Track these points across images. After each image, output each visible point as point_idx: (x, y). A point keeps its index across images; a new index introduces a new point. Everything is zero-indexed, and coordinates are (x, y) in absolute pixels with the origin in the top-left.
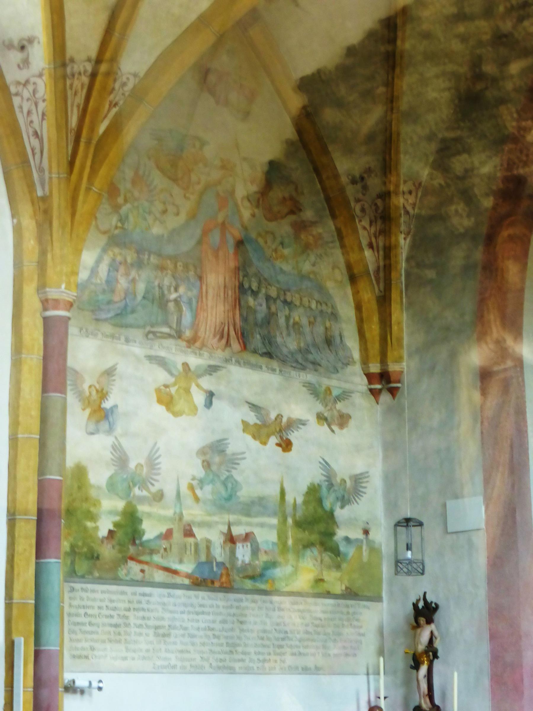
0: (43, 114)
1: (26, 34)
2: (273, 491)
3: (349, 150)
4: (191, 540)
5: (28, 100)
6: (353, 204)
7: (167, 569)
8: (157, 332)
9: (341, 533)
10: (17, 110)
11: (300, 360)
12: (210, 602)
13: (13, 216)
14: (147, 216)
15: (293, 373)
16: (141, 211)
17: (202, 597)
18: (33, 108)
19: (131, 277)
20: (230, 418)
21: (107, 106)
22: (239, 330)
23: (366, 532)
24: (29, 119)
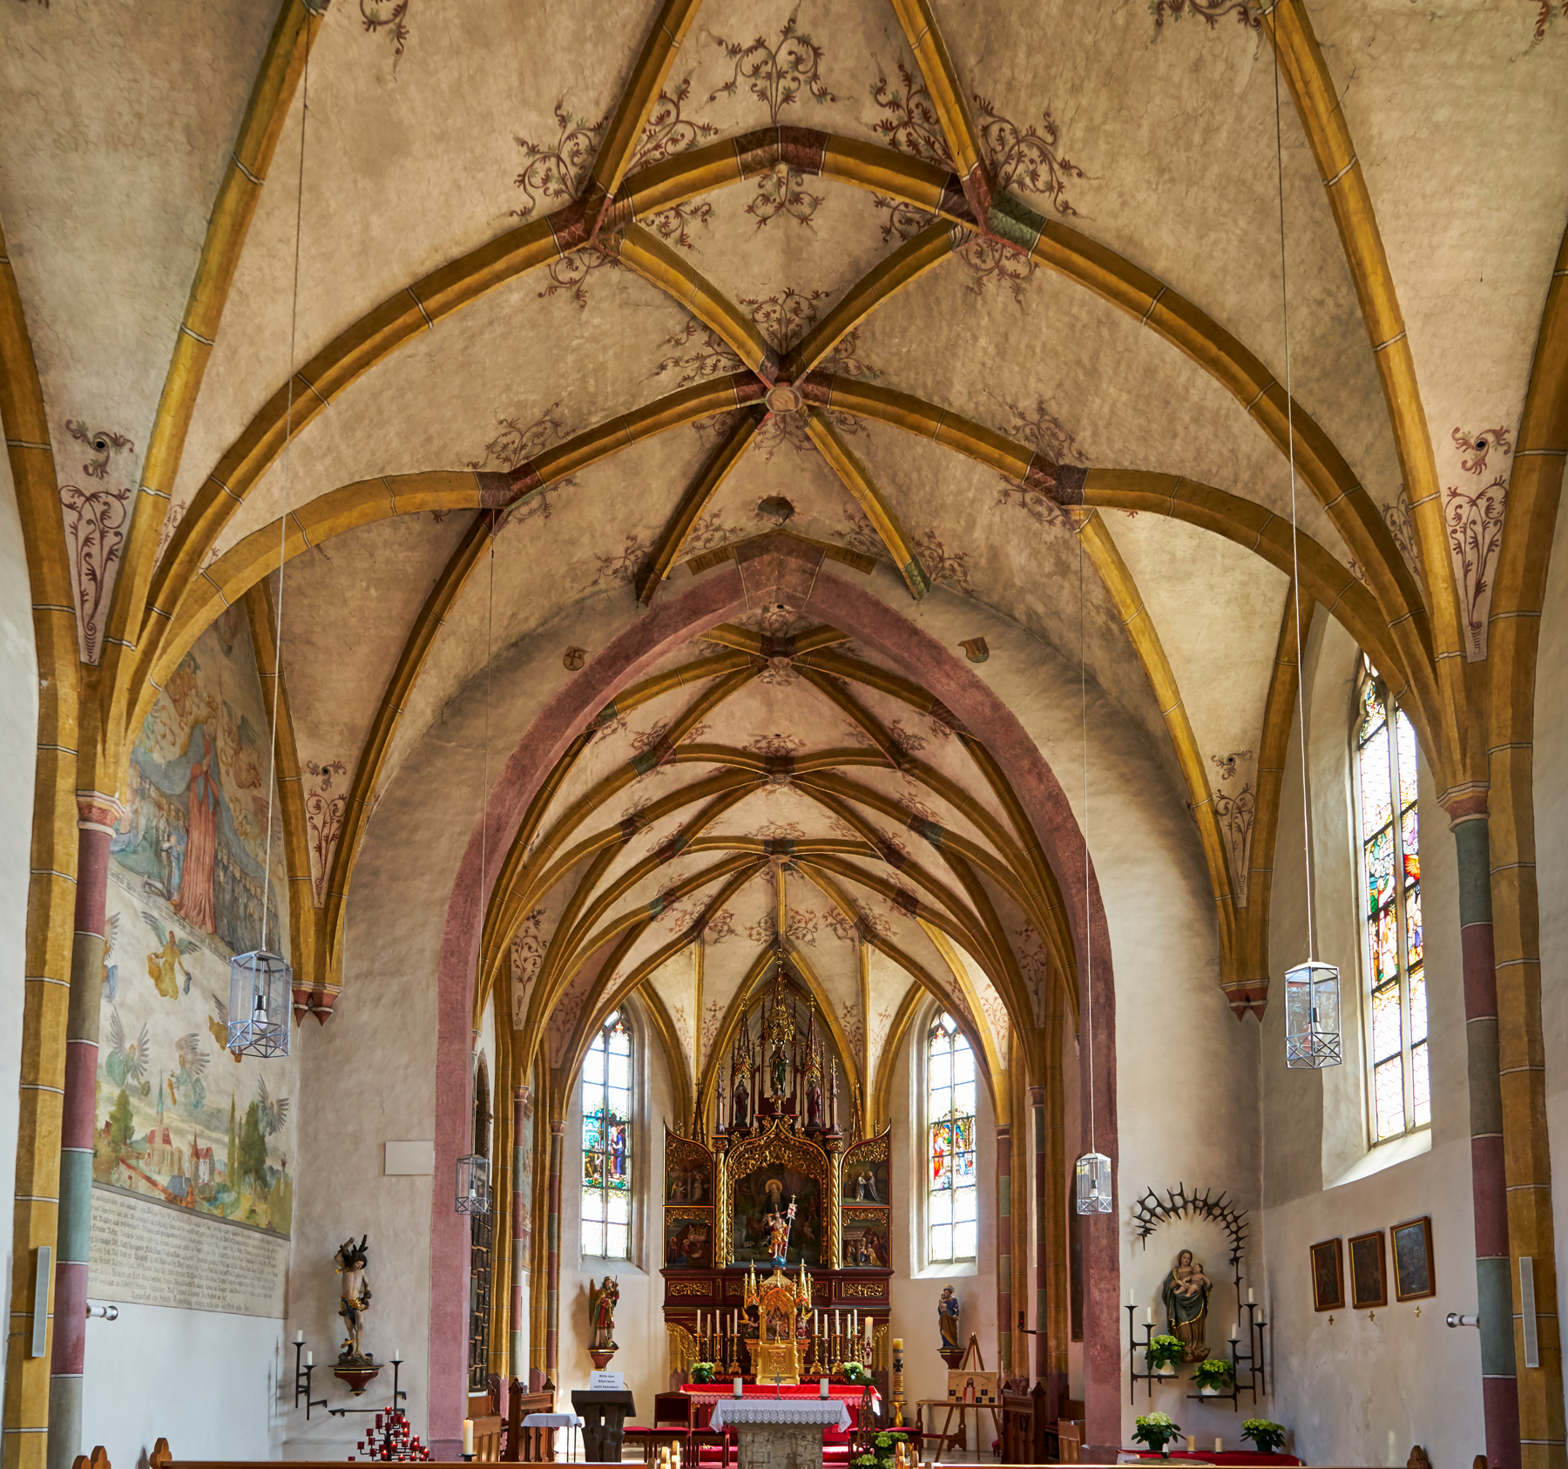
0: (111, 552)
1: (117, 430)
2: (225, 1104)
3: (314, 732)
4: (167, 1147)
5: (90, 522)
6: (306, 796)
7: (148, 1179)
9: (269, 1162)
10: (68, 530)
12: (177, 1224)
13: (42, 676)
17: (171, 1216)
18: (97, 535)
20: (200, 1009)
23: (284, 1164)
24: (86, 550)
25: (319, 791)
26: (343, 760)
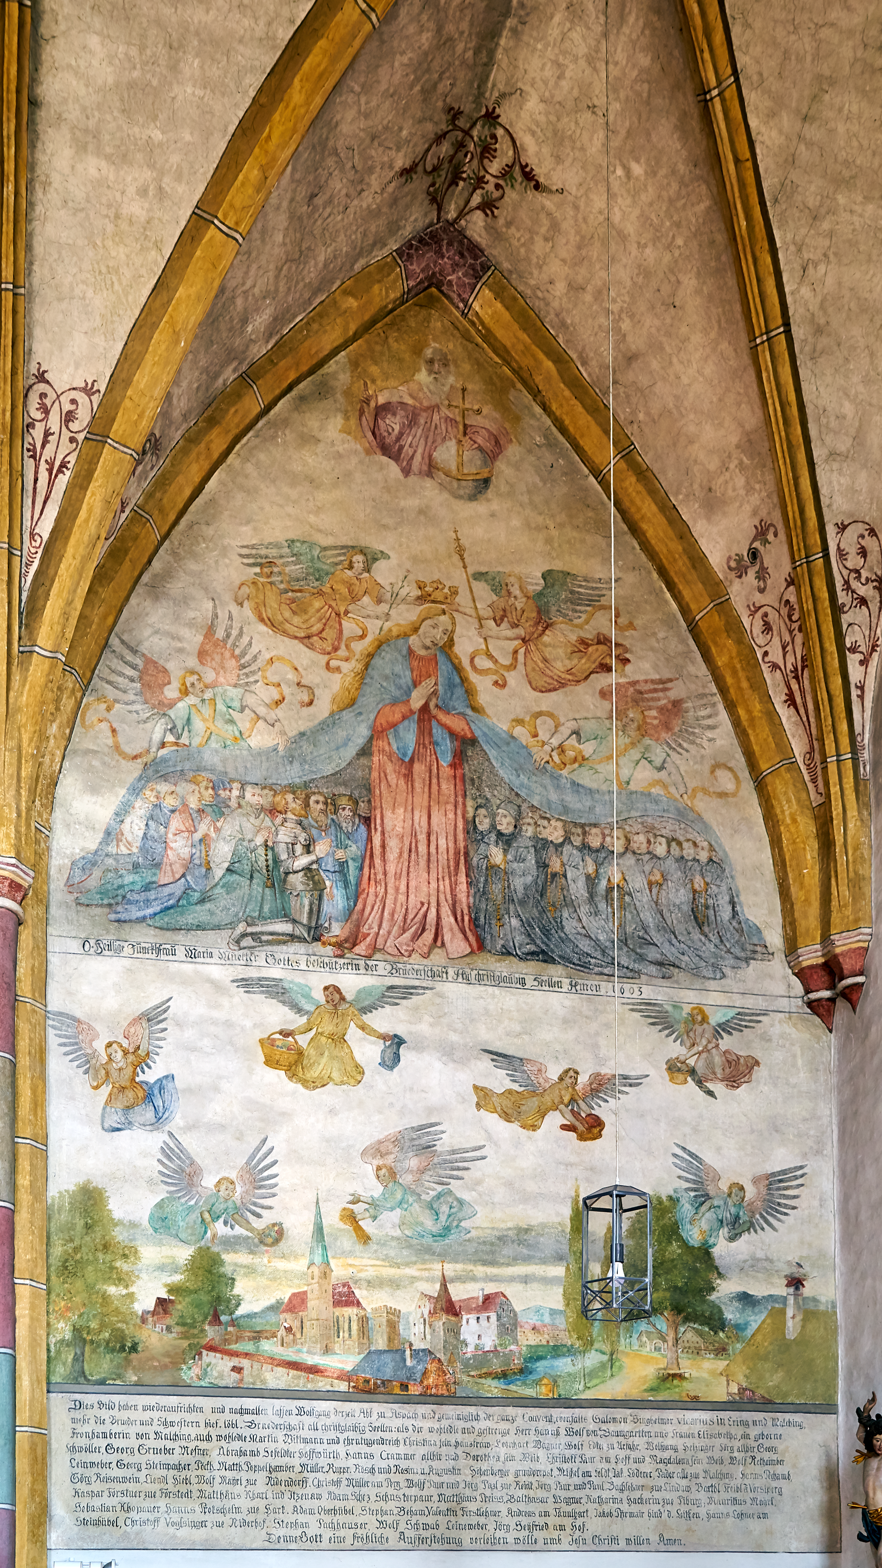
8: (262, 933)
14: (235, 715)
15: (605, 987)
16: (221, 707)
19: (197, 836)
21: (43, 476)
22: (466, 911)
26: (763, 513)
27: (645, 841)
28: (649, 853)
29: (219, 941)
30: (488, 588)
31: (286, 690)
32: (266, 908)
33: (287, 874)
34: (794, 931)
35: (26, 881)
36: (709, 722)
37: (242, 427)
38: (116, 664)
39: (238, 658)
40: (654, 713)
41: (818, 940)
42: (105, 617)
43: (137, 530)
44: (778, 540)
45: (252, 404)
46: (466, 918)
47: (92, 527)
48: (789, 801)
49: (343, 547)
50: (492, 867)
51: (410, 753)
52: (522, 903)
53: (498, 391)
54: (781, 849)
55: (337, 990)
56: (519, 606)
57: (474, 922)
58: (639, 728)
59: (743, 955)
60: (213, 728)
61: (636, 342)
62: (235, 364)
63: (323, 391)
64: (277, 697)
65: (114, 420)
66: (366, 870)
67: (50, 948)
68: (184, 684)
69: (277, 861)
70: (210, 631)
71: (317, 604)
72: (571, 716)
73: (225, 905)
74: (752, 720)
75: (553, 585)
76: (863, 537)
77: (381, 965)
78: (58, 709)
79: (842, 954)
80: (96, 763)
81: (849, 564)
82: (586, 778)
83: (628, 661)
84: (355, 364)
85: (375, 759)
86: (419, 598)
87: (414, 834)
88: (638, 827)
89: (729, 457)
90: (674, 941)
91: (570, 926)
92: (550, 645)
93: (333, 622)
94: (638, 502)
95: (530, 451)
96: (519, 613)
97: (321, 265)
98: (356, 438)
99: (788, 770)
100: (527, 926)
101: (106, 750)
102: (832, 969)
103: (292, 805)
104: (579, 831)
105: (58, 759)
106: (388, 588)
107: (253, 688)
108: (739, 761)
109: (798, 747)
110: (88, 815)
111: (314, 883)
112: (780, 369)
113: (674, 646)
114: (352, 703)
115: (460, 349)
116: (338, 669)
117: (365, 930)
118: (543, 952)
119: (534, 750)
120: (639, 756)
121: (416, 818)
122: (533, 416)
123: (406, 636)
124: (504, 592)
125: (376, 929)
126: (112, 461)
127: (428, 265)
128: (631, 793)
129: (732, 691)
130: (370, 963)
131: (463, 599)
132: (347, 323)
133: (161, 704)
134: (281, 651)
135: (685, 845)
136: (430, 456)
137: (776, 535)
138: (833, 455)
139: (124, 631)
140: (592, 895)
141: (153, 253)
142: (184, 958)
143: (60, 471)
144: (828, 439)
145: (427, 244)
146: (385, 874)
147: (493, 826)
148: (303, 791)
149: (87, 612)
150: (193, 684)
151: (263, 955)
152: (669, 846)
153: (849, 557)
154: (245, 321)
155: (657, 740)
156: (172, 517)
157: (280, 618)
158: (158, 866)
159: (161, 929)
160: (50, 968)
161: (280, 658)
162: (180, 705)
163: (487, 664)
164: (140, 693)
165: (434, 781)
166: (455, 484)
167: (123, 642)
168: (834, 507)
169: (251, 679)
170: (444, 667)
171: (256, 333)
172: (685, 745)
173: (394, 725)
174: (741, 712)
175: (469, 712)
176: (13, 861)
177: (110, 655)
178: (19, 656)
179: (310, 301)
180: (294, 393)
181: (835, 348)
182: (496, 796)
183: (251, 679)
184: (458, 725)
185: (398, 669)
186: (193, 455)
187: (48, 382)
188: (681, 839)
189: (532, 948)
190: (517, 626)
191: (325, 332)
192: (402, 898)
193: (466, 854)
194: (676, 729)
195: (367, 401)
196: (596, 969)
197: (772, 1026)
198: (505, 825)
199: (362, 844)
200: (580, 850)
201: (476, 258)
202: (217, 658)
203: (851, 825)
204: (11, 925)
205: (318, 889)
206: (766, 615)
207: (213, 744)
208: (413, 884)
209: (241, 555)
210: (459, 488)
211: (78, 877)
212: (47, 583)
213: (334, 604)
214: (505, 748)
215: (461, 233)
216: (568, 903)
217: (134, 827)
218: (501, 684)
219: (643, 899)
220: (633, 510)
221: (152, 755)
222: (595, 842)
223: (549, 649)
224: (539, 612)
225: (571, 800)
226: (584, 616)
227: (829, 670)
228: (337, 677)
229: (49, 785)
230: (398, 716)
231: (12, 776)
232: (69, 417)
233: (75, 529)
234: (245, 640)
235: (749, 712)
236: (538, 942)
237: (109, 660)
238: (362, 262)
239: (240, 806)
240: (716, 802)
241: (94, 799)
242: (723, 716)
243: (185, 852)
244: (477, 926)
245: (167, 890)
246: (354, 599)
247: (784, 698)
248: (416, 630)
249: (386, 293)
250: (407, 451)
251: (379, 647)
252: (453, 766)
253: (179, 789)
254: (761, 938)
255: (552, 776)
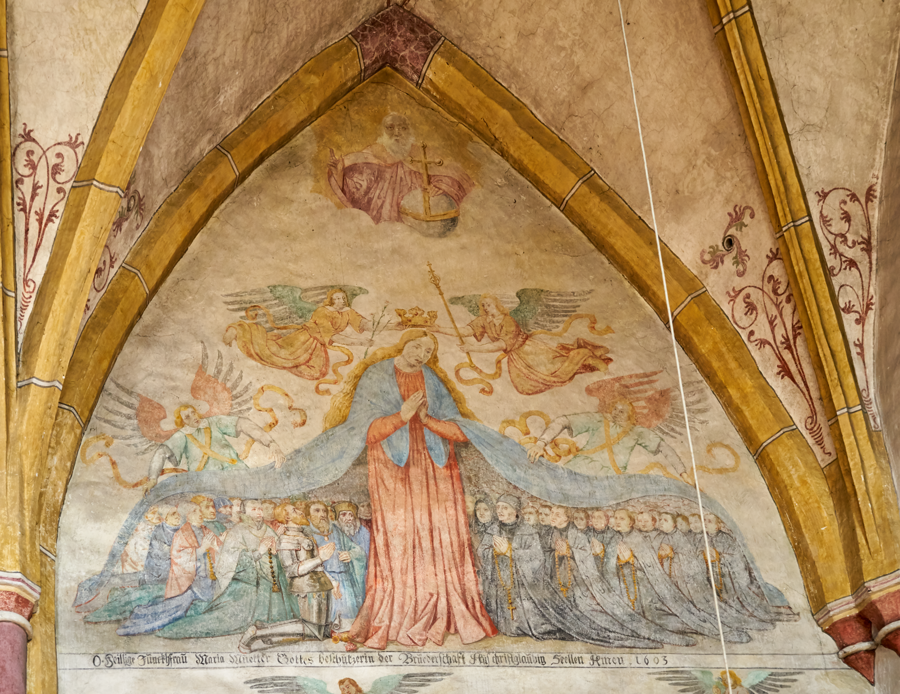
6: (726, 308)
8: (273, 635)
11: (644, 632)
14: (231, 440)
15: (629, 659)
16: (216, 434)
19: (201, 551)
21: (34, 226)
22: (476, 598)
25: (739, 283)
26: (737, 198)
27: (650, 519)
28: (655, 529)
29: (230, 646)
30: (465, 309)
31: (279, 414)
32: (275, 611)
33: (293, 578)
34: (820, 588)
35: (33, 596)
36: (700, 406)
37: (219, 191)
38: (112, 404)
39: (230, 390)
40: (642, 403)
41: (849, 592)
42: (100, 361)
43: (126, 284)
44: (755, 221)
45: (228, 172)
46: (478, 605)
47: (83, 264)
48: (795, 465)
49: (323, 288)
50: (498, 556)
51: (405, 459)
52: (533, 586)
53: (457, 145)
54: (792, 513)
55: (353, 683)
56: (497, 322)
57: (486, 608)
58: (629, 418)
59: (767, 617)
60: (210, 453)
61: (589, 70)
62: (209, 135)
63: (293, 161)
64: (270, 420)
65: (98, 163)
66: (372, 568)
67: (60, 666)
68: (179, 417)
69: (281, 567)
70: (201, 370)
71: (303, 337)
72: (560, 413)
73: (233, 612)
74: (744, 397)
75: (528, 302)
76: (845, 202)
77: (395, 655)
78: (58, 443)
79: (880, 600)
80: (98, 493)
81: (833, 229)
82: (582, 467)
83: (611, 360)
84: (320, 136)
85: (371, 467)
86: (399, 324)
87: (416, 532)
88: (640, 507)
89: (696, 153)
90: (693, 609)
91: (584, 604)
92: (532, 353)
93: (320, 351)
94: (603, 219)
95: (492, 192)
96: (498, 328)
97: (284, 42)
98: (326, 195)
99: (790, 437)
100: (540, 607)
101: (107, 481)
102: (868, 619)
103: (293, 515)
104: (582, 515)
105: (60, 490)
106: (369, 318)
107: (246, 415)
108: (735, 438)
109: (798, 414)
110: (90, 541)
111: (321, 584)
112: (749, 47)
113: (654, 343)
114: (344, 420)
115: (417, 114)
116: (327, 392)
117: (376, 623)
118: (560, 630)
119: (527, 447)
120: (633, 443)
121: (417, 517)
122: (493, 162)
123: (390, 357)
124: (481, 312)
125: (387, 622)
126: (101, 204)
127: (381, 44)
128: (630, 477)
129: (720, 374)
130: (384, 654)
131: (443, 321)
132: (311, 98)
133: (158, 436)
134: (271, 381)
135: (691, 519)
136: (398, 204)
137: (752, 216)
138: (806, 127)
139: (119, 376)
140: (603, 575)
141: (128, 11)
142: (195, 665)
143: (49, 220)
144: (801, 112)
145: (380, 25)
146: (391, 570)
147: (495, 518)
148: (304, 503)
149: (82, 356)
150: (188, 417)
151: (275, 656)
152: (675, 522)
153: (833, 223)
154: (217, 91)
155: (649, 427)
156: (159, 273)
157: (268, 352)
158: (164, 581)
159: (170, 639)
160: (61, 684)
161: (271, 387)
162: (177, 435)
163: (473, 375)
164: (138, 428)
165: (432, 482)
166: (424, 225)
167: (118, 385)
168: (813, 175)
169: (244, 407)
170: (430, 381)
171: (228, 105)
172: (677, 429)
173: (386, 436)
174: (732, 391)
175: (459, 417)
176: (19, 576)
177: (107, 398)
178: (17, 390)
179: (274, 79)
180: (266, 163)
181: (800, 26)
182: (494, 491)
183: (244, 407)
184: (450, 430)
185: (386, 386)
186: (175, 217)
187: (34, 140)
188: (687, 514)
189: (549, 627)
190: (498, 339)
191: (291, 107)
192: (410, 591)
193: (471, 546)
194: (667, 416)
195: (335, 165)
196: (617, 643)
197: (809, 683)
198: (507, 516)
199: (365, 545)
200: (585, 533)
201: (426, 32)
202: (210, 392)
203: (870, 475)
204: (19, 639)
205: (325, 590)
206: (748, 296)
207: (211, 467)
208: (419, 577)
209: (226, 303)
210: (428, 228)
211: (85, 596)
212: (42, 321)
213: (318, 336)
214: (498, 447)
215: (411, 13)
216: (579, 582)
217: (138, 548)
218: (488, 391)
219: (656, 573)
220: (599, 228)
221: (152, 482)
222: (600, 524)
223: (531, 357)
224: (517, 326)
225: (569, 487)
226: (561, 326)
227: (827, 327)
228: (327, 398)
229: (53, 513)
230: (389, 427)
231: (14, 498)
232: (56, 170)
233: (66, 267)
234: (236, 374)
235: (740, 389)
236: (554, 621)
237: (105, 402)
238: (321, 43)
239: (241, 520)
240: (716, 478)
241: (97, 525)
242: (713, 400)
243: (190, 566)
244: (489, 611)
245: (174, 603)
246: (338, 330)
247: (777, 370)
248: (400, 351)
249: (346, 70)
250: (376, 202)
251: (365, 369)
252: (449, 467)
253: (180, 510)
254: (783, 600)
255: (548, 468)
